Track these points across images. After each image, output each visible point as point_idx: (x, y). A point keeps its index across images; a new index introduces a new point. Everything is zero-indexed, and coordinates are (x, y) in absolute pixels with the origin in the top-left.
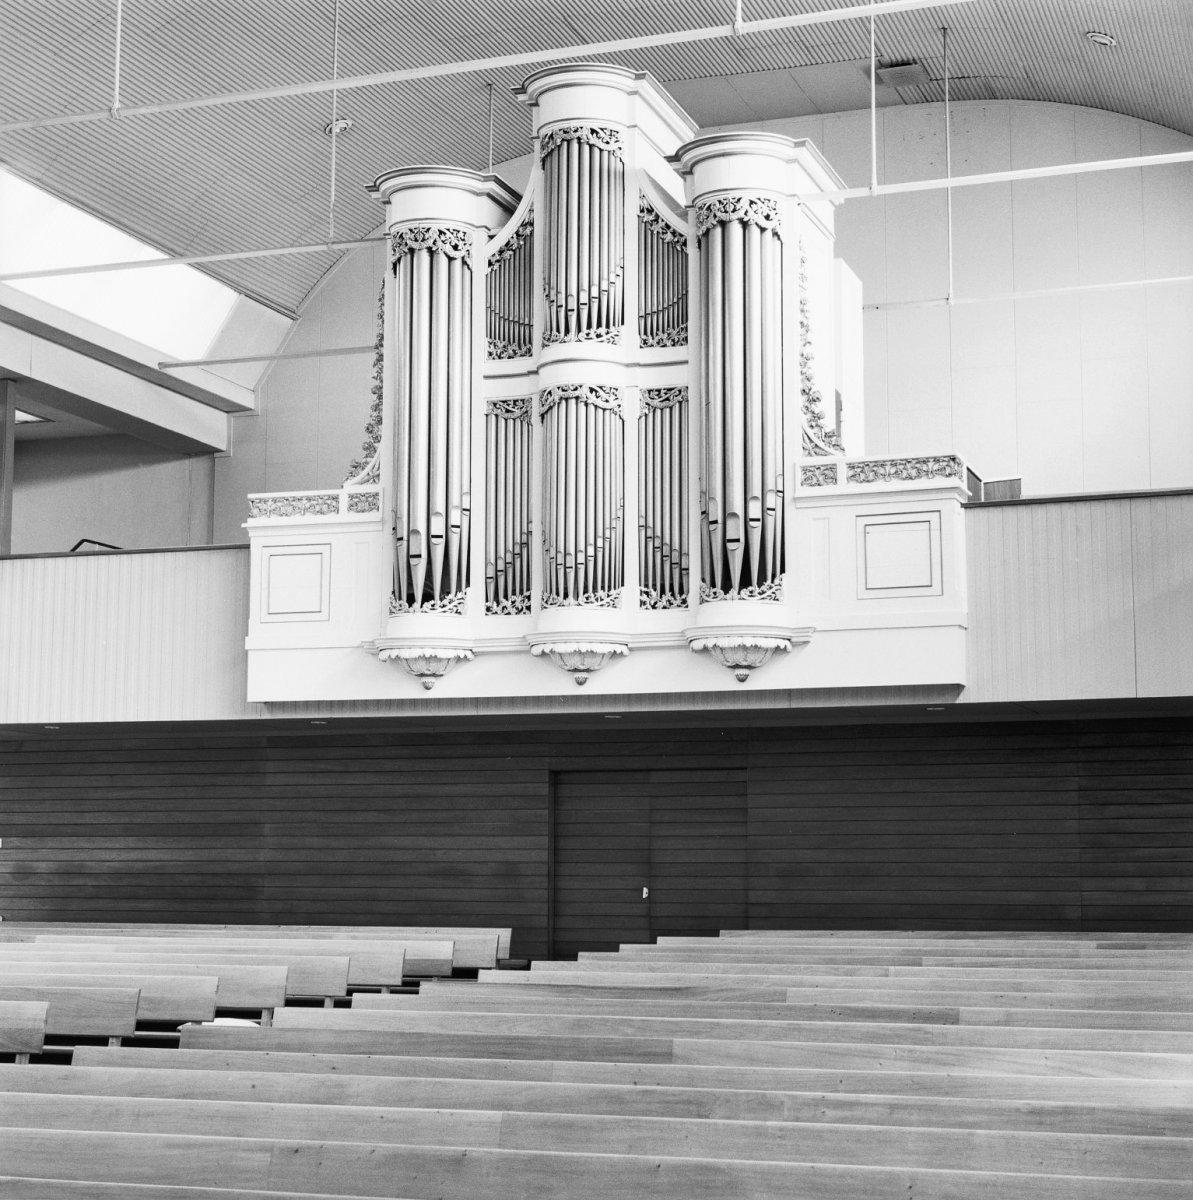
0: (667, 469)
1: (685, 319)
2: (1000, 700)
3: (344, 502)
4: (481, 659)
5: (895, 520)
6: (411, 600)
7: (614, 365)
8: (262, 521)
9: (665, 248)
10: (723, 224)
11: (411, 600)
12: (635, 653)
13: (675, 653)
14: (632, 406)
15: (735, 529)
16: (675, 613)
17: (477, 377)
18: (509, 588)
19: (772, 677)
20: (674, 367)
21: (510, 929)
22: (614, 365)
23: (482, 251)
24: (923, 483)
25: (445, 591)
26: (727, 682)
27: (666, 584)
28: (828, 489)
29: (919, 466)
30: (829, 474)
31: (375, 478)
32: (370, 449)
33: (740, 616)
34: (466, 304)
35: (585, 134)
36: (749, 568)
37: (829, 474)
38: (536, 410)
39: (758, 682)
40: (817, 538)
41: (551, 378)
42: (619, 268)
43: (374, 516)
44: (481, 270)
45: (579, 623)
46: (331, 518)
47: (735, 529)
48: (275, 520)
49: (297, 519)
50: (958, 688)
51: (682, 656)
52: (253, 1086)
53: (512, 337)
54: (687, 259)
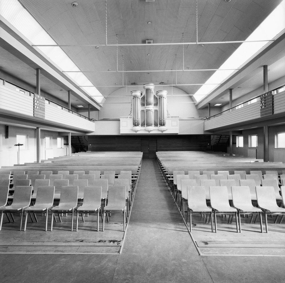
0: (143, 117)
1: (157, 104)
2: (108, 135)
3: (129, 117)
4: (141, 130)
5: (174, 121)
6: (160, 125)
7: (152, 108)
8: (121, 119)
9: (155, 98)
10: (162, 97)
11: (162, 125)
12: (153, 130)
13: (157, 131)
14: (153, 111)
15: (136, 121)
16: (157, 127)
17: (140, 108)
18: (143, 125)
19: (164, 133)
20: (157, 108)
21: (142, 153)
22: (152, 108)
23: (140, 98)
24: (173, 118)
25: (138, 125)
26: (161, 133)
27: (156, 125)
28: (169, 118)
29: (176, 117)
30: (169, 117)
31: (131, 116)
32: (131, 113)
33: (162, 128)
34: (139, 102)
35: (150, 89)
36: (162, 124)
37: (169, 117)
38: (145, 111)
39: (163, 133)
40: (168, 122)
41: (147, 109)
42: (152, 100)
43: (131, 119)
44: (140, 99)
45: (150, 128)
46: (127, 119)
47: (136, 121)
48: (122, 119)
49: (124, 119)
50: (178, 133)
51: (158, 131)
52: (261, 185)
53: (143, 105)
54: (158, 100)
